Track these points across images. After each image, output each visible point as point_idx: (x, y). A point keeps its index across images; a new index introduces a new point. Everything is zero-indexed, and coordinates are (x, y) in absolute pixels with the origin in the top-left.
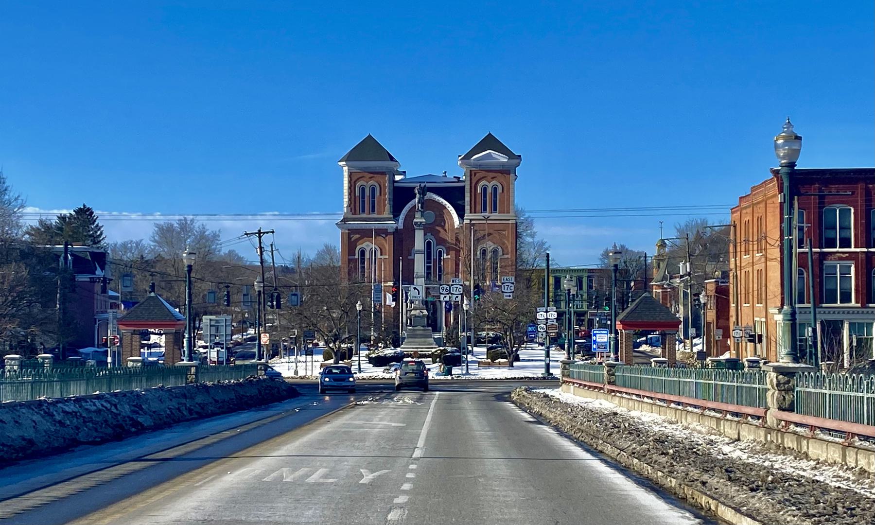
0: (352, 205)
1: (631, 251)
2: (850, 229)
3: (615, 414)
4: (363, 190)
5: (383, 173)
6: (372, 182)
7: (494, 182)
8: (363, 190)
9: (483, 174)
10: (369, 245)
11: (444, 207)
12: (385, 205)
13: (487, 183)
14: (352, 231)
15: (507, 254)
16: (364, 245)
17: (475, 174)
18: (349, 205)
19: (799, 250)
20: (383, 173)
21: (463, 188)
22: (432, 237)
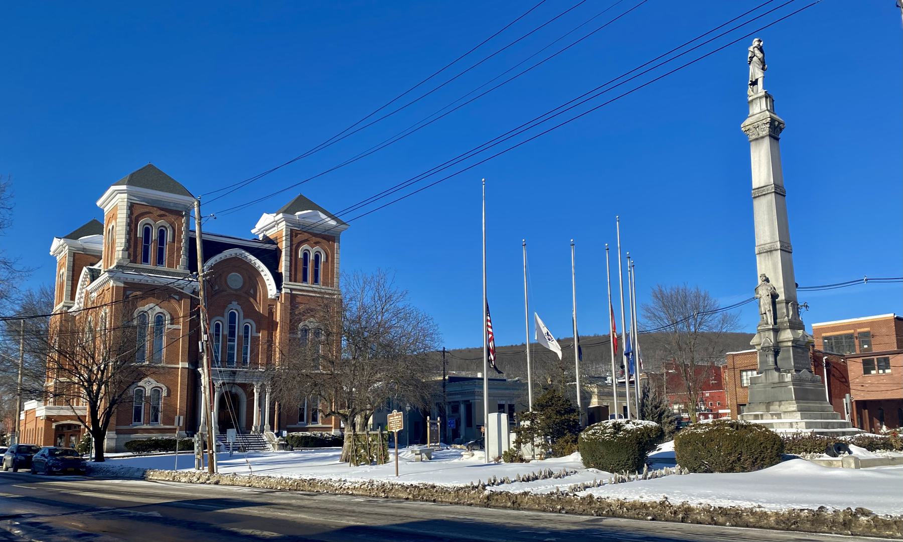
0: (132, 250)
1: (454, 351)
2: (489, 395)
3: (434, 487)
4: (147, 231)
5: (178, 214)
6: (161, 222)
7: (317, 248)
8: (147, 231)
9: (306, 236)
10: (151, 309)
11: (256, 273)
12: (179, 256)
13: (309, 248)
14: (130, 286)
15: (178, 323)
16: (146, 308)
17: (296, 236)
18: (127, 249)
19: (169, 326)
20: (178, 214)
21: (278, 252)
22: (239, 308)
